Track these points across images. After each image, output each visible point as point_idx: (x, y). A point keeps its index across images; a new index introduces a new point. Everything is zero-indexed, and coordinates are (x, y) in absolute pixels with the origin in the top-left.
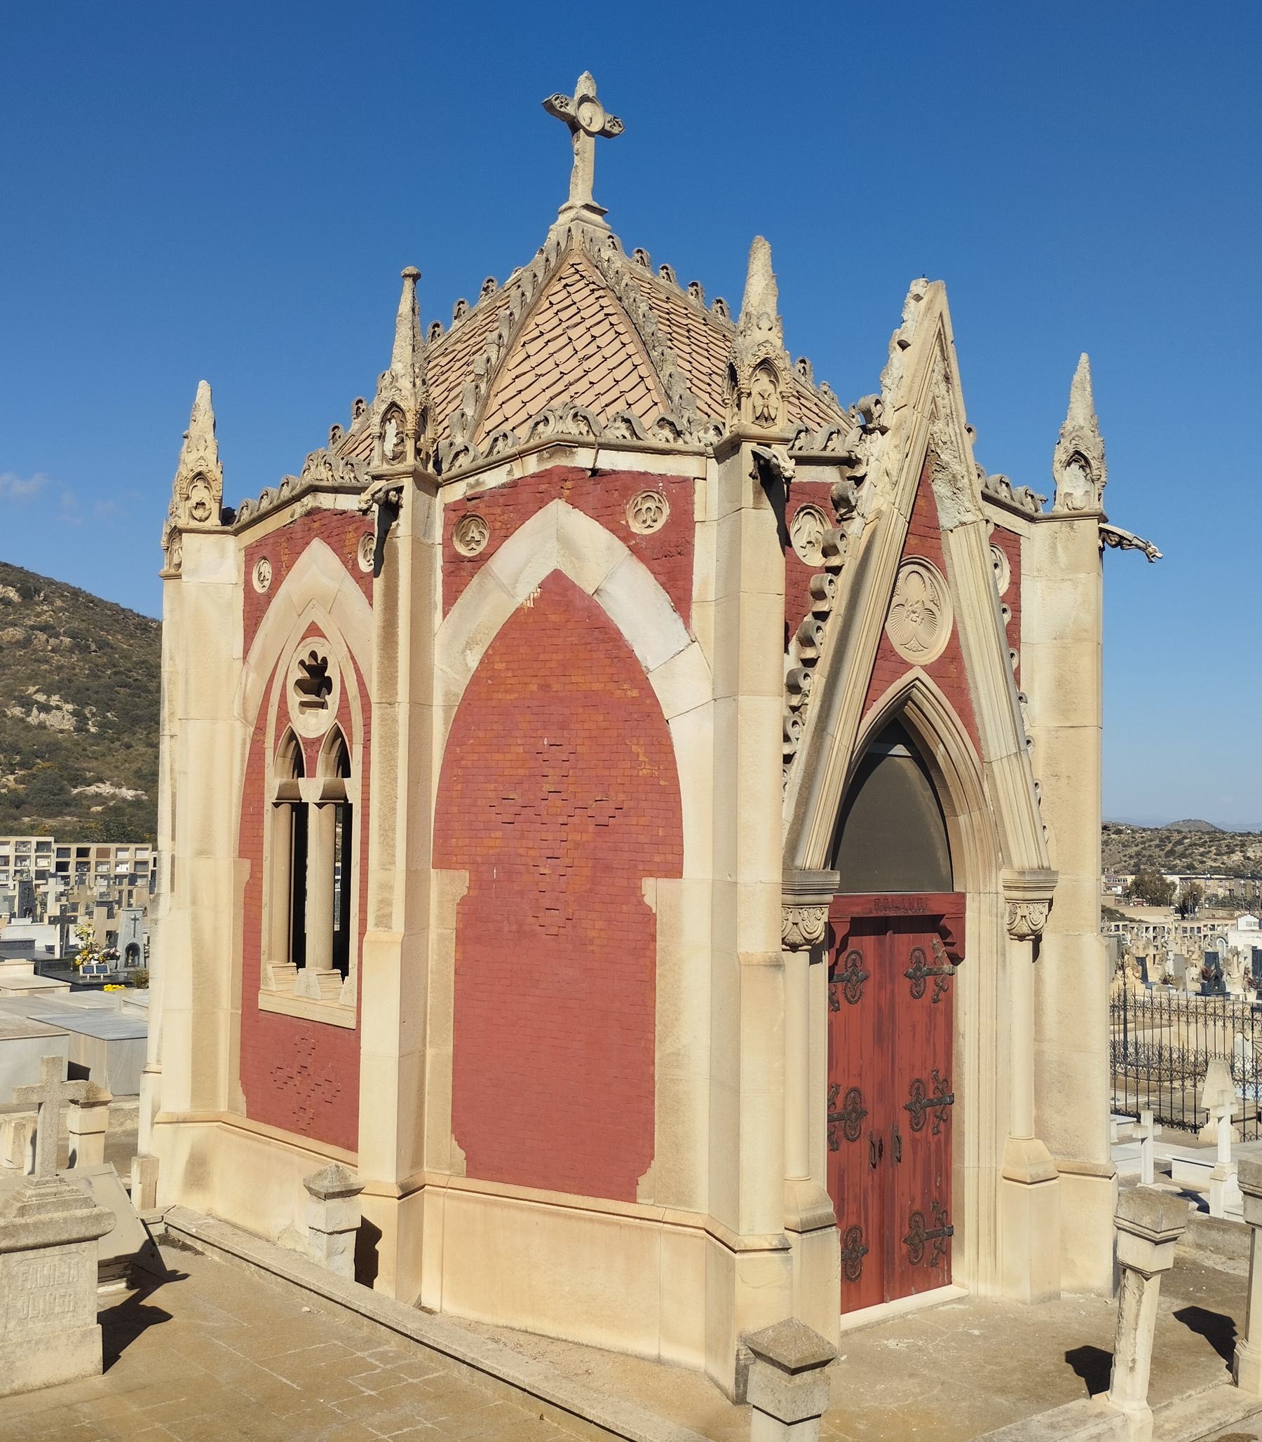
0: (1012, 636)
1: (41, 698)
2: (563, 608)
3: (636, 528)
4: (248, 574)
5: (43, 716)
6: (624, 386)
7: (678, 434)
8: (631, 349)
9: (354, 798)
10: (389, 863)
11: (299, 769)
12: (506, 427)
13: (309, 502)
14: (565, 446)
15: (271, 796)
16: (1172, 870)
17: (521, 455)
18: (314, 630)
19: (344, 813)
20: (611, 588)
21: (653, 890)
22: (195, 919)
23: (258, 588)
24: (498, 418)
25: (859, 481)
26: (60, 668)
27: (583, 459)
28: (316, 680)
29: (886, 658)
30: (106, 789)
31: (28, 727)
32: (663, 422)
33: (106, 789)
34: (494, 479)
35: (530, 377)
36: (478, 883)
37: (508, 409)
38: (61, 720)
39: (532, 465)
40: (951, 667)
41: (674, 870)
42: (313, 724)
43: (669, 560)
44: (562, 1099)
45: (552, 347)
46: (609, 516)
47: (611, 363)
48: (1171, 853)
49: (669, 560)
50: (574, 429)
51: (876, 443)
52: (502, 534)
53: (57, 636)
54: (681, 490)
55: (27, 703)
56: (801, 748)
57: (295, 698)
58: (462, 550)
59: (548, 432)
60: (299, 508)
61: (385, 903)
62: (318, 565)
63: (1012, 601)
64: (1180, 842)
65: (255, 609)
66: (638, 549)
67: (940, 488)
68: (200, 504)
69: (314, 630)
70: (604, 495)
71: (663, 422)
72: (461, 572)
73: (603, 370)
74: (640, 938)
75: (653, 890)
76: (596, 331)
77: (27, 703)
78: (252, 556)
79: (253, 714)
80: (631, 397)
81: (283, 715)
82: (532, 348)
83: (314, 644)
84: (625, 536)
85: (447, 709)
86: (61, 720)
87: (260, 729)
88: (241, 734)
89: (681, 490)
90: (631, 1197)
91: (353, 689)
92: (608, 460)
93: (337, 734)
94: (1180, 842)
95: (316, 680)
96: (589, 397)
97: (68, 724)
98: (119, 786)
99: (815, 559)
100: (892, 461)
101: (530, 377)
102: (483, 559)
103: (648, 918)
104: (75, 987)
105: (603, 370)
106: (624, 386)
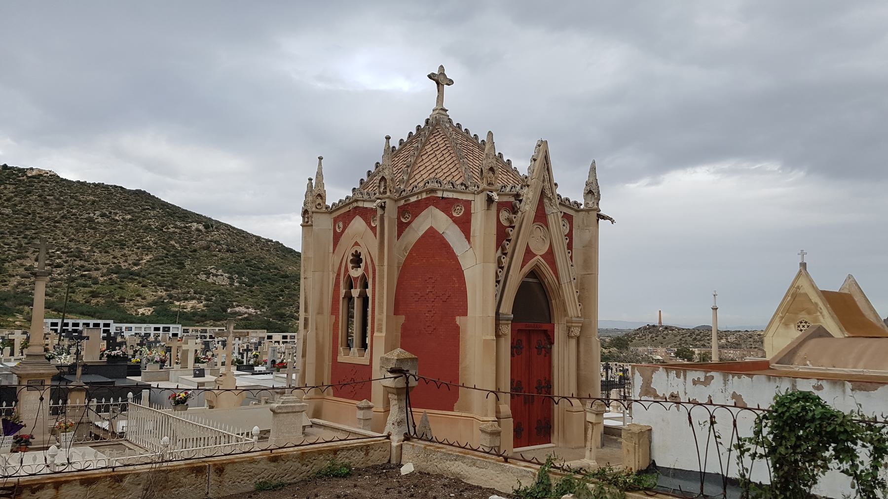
0: (570, 246)
1: (214, 271)
2: (432, 235)
3: (455, 214)
4: (334, 226)
5: (215, 278)
6: (452, 170)
7: (467, 187)
8: (454, 158)
9: (369, 295)
10: (381, 312)
11: (351, 287)
12: (415, 183)
13: (355, 205)
14: (433, 191)
15: (342, 295)
16: (696, 346)
17: (421, 192)
18: (356, 244)
19: (365, 299)
20: (447, 232)
21: (459, 320)
22: (317, 334)
23: (338, 231)
24: (413, 180)
25: (521, 201)
26: (222, 259)
27: (439, 194)
28: (357, 260)
29: (529, 254)
30: (242, 309)
31: (209, 284)
32: (462, 184)
33: (242, 309)
34: (413, 199)
35: (423, 167)
36: (407, 319)
37: (417, 177)
38: (222, 280)
39: (424, 196)
40: (550, 256)
41: (465, 313)
42: (356, 273)
43: (464, 224)
44: (431, 382)
45: (431, 157)
46: (447, 211)
47: (449, 163)
48: (695, 339)
49: (464, 224)
50: (436, 185)
51: (525, 190)
52: (415, 216)
53: (220, 245)
54: (467, 204)
55: (208, 274)
56: (502, 279)
57: (350, 265)
58: (403, 220)
59: (429, 186)
60: (351, 206)
61: (380, 325)
62: (358, 223)
63: (570, 235)
64: (698, 335)
65: (337, 237)
66: (456, 221)
67: (546, 200)
68: (319, 204)
69: (356, 244)
70: (446, 205)
71: (462, 184)
72: (402, 227)
73: (446, 165)
74: (454, 335)
75: (459, 320)
76: (444, 152)
77: (208, 274)
78: (336, 221)
79: (336, 270)
80: (454, 174)
81: (346, 270)
82: (424, 157)
83: (357, 248)
84: (451, 217)
85: (398, 267)
86: (222, 280)
87: (338, 275)
88: (332, 276)
89: (467, 204)
90: (453, 411)
91: (369, 262)
92: (446, 195)
93: (364, 275)
94: (698, 335)
95: (357, 260)
96: (441, 174)
97: (226, 282)
98: (248, 308)
99: (505, 223)
100: (530, 195)
101: (423, 167)
102: (410, 223)
103: (458, 328)
104: (253, 374)
105: (446, 165)
106: (452, 170)
